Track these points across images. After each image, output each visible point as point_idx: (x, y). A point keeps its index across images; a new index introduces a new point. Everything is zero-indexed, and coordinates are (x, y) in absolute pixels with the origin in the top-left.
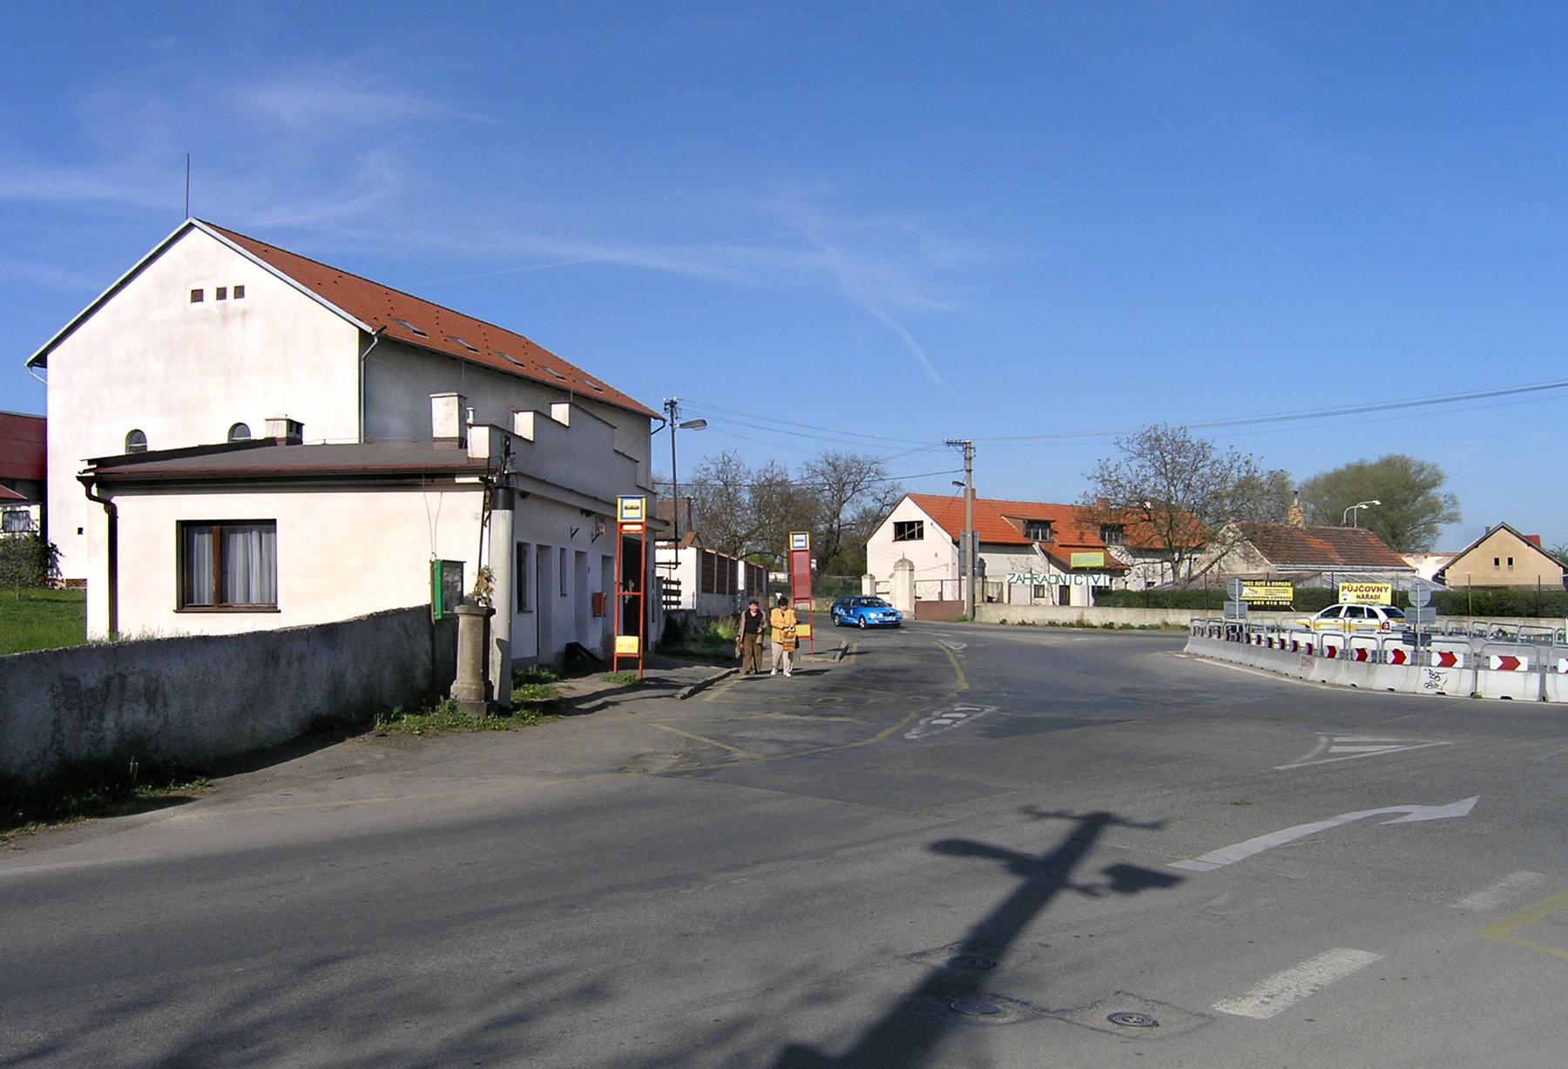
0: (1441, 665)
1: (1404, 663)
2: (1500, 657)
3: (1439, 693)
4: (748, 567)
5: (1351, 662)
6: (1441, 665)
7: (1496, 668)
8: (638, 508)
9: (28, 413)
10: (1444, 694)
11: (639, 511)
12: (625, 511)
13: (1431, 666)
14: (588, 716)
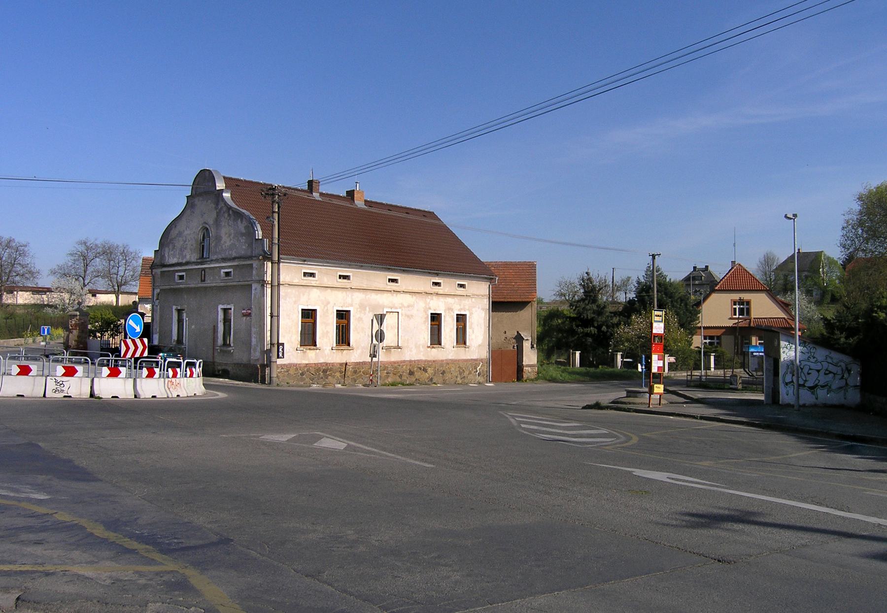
0: (64, 375)
1: (154, 377)
2: (64, 367)
3: (65, 396)
4: (625, 358)
5: (185, 378)
6: (64, 375)
7: (105, 376)
8: (661, 316)
9: (752, 294)
10: (70, 397)
11: (661, 318)
12: (655, 317)
13: (56, 376)
14: (674, 412)
